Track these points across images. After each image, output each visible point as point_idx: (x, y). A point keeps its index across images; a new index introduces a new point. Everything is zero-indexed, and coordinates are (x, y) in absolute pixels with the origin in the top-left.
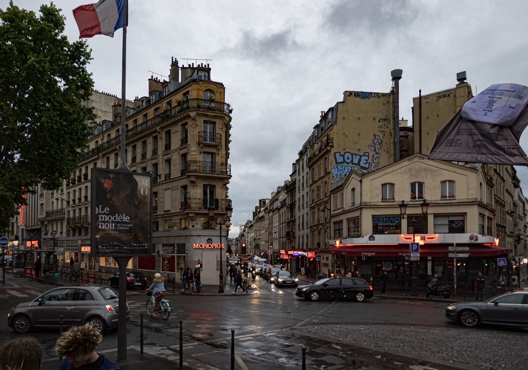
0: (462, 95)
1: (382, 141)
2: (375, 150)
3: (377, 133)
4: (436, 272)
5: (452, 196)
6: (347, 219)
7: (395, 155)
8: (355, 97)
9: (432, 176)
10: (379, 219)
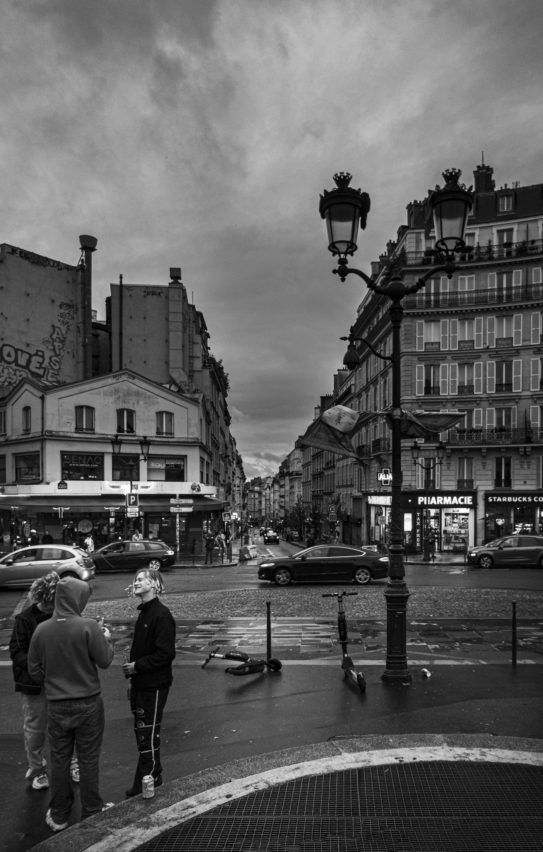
0: (176, 298)
1: (65, 338)
2: (54, 350)
3: (58, 324)
4: (151, 532)
5: (170, 433)
6: (13, 454)
7: (85, 363)
8: (21, 259)
9: (145, 403)
10: (71, 458)
